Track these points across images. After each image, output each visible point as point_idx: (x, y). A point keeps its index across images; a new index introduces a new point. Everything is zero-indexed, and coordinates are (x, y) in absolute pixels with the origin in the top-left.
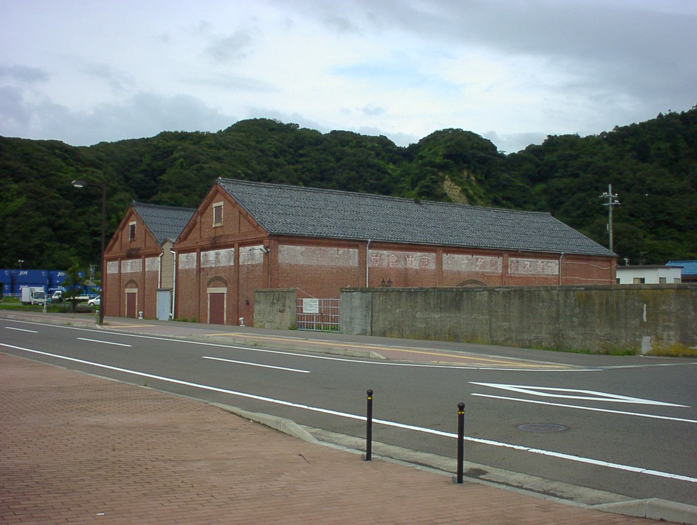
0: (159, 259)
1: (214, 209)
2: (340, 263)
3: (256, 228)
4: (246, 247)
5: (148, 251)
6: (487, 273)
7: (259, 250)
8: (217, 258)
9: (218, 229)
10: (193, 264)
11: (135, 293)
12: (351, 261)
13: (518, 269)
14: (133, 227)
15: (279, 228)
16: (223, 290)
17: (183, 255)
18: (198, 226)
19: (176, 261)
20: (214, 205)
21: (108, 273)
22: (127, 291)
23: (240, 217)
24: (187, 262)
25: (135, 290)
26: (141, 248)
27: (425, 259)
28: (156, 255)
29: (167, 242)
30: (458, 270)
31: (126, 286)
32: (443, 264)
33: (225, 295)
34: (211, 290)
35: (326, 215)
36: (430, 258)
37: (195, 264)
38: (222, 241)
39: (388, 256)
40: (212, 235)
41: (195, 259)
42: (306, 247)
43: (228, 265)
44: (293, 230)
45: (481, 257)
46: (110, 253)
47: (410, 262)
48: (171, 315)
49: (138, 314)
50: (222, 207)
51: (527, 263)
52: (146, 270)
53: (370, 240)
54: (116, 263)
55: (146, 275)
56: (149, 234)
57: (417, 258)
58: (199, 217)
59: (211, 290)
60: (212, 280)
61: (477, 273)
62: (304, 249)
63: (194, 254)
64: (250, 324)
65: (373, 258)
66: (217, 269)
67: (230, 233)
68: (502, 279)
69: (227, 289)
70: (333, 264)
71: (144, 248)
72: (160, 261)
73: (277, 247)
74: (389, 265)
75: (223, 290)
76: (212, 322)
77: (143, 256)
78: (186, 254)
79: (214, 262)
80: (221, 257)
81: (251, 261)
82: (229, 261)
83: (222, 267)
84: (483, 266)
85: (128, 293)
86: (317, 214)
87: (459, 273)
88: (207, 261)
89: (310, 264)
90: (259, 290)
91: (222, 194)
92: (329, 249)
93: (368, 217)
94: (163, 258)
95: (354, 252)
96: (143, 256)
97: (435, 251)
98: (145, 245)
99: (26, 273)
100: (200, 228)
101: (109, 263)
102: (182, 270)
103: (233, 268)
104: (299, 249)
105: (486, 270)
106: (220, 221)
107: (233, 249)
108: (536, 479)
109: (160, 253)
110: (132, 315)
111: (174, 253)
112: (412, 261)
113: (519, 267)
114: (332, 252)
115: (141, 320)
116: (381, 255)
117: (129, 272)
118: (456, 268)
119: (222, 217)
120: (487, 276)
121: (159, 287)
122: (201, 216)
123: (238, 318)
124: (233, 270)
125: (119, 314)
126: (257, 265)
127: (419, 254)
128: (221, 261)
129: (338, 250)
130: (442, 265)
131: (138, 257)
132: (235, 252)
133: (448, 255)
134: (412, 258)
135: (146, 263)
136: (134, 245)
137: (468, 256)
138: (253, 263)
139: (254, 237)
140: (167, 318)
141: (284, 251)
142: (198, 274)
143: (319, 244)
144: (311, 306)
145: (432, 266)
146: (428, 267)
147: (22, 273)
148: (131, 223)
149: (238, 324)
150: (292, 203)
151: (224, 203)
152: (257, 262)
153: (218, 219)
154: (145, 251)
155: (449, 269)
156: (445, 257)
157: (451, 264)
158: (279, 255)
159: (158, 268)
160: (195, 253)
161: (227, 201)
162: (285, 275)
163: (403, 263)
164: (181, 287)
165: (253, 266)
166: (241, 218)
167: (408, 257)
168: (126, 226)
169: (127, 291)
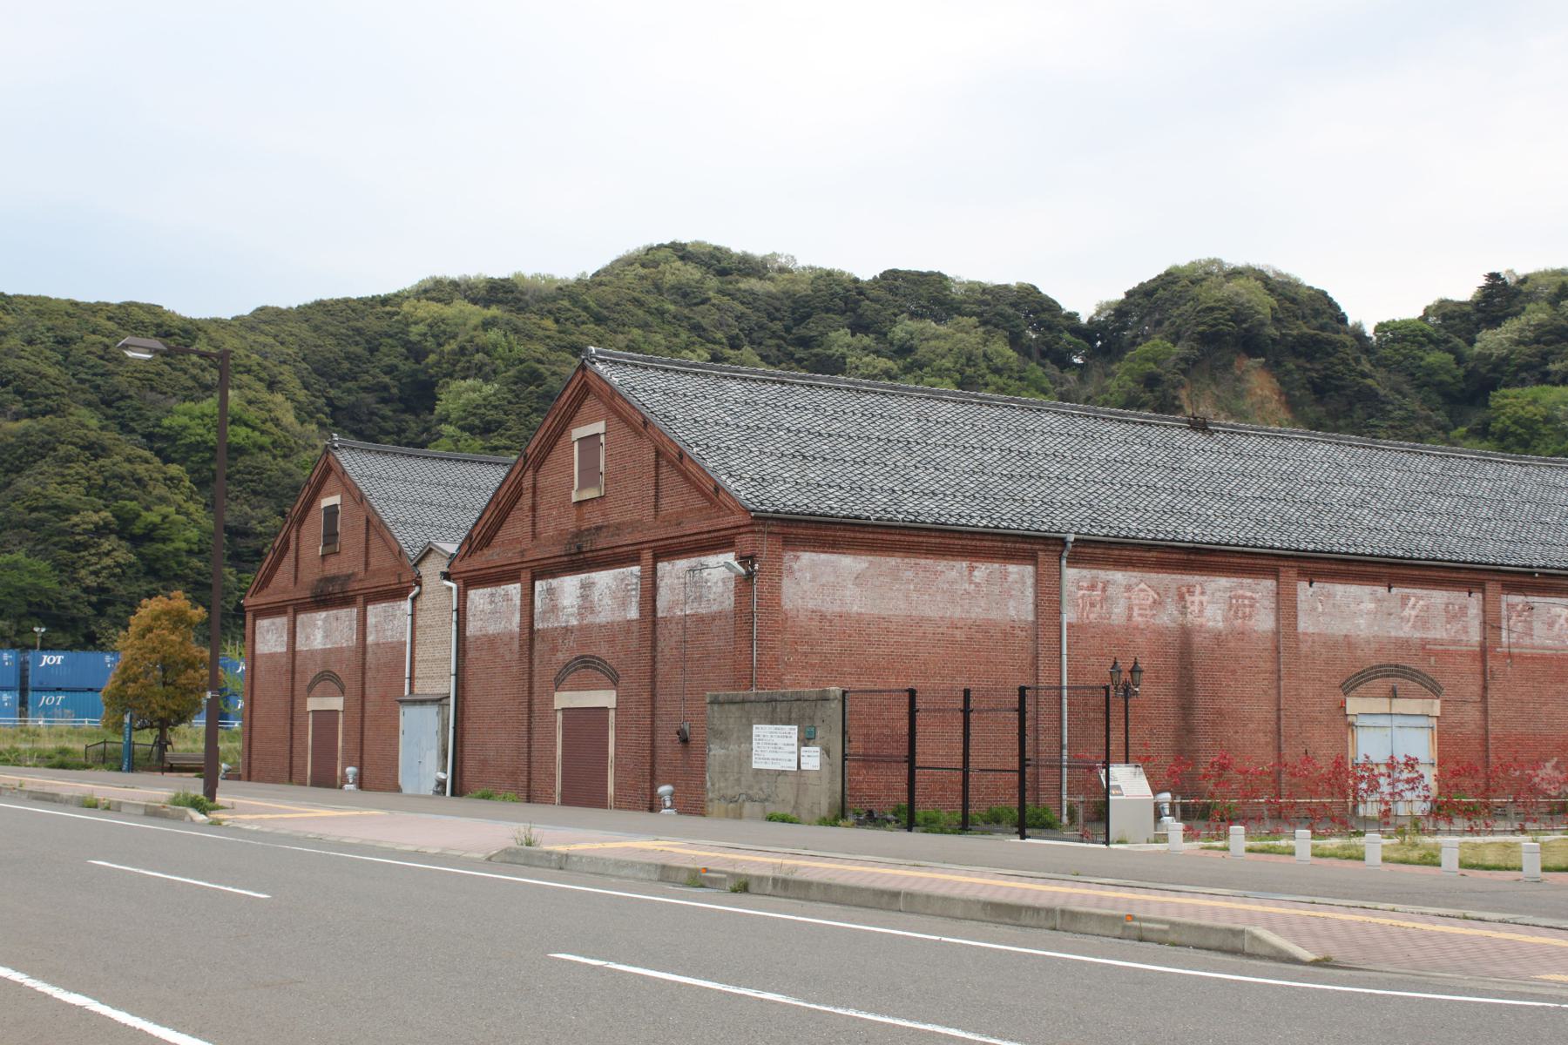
0: (406, 605)
1: (576, 445)
2: (978, 611)
3: (710, 500)
4: (677, 562)
5: (374, 582)
6: (1435, 641)
7: (720, 568)
8: (584, 597)
9: (586, 509)
10: (509, 621)
11: (336, 711)
12: (1012, 603)
13: (1531, 629)
14: (331, 512)
15: (785, 496)
16: (605, 698)
17: (481, 591)
18: (526, 500)
19: (457, 610)
20: (578, 433)
21: (257, 652)
22: (313, 704)
23: (657, 466)
24: (493, 612)
25: (336, 703)
26: (353, 574)
27: (1244, 597)
28: (397, 594)
29: (432, 555)
30: (1344, 632)
31: (310, 691)
32: (1300, 614)
33: (612, 714)
34: (565, 699)
35: (925, 463)
36: (1256, 596)
37: (517, 618)
38: (602, 542)
39: (1129, 588)
40: (570, 524)
41: (518, 602)
42: (870, 558)
43: (620, 619)
44: (833, 504)
45: (1418, 592)
46: (265, 592)
47: (1196, 608)
48: (443, 776)
49: (344, 775)
50: (602, 439)
51: (1558, 610)
52: (371, 639)
53: (1071, 538)
54: (282, 622)
55: (369, 656)
56: (378, 533)
57: (1218, 594)
58: (530, 473)
59: (565, 699)
60: (568, 668)
61: (1403, 644)
62: (867, 565)
63: (514, 589)
64: (692, 805)
65: (1081, 592)
66: (584, 630)
67: (627, 518)
68: (1484, 661)
69: (617, 696)
70: (957, 613)
71: (362, 575)
72: (409, 612)
73: (780, 558)
74: (1130, 618)
75: (605, 698)
76: (569, 799)
77: (360, 600)
78: (489, 590)
79: (575, 610)
80: (597, 594)
81: (695, 604)
82: (624, 605)
83: (600, 626)
84: (1423, 621)
85: (313, 711)
86: (898, 456)
87: (1349, 644)
88: (554, 609)
89: (885, 613)
90: (723, 694)
91: (600, 398)
92: (942, 565)
93: (1055, 469)
94: (418, 605)
95: (1020, 575)
96: (360, 600)
97: (1274, 573)
98: (367, 564)
99: (58, 659)
100: (534, 508)
101: (263, 624)
102: (478, 638)
103: (635, 628)
104: (850, 563)
105: (1430, 635)
106: (595, 484)
107: (636, 569)
108: (44, 566)
109: (412, 588)
110: (326, 779)
111: (453, 585)
112: (1201, 603)
113: (1534, 624)
114: (954, 574)
115: (350, 791)
116: (1106, 584)
117: (320, 647)
118: (1338, 628)
119: (602, 469)
120: (1436, 654)
121: (407, 693)
122: (536, 471)
123: (653, 788)
124: (636, 635)
125: (289, 775)
126: (714, 617)
127: (1223, 582)
128: (598, 609)
129: (972, 569)
130: (1296, 617)
131: (345, 601)
132: (641, 578)
133: (1314, 584)
134: (1203, 593)
135: (371, 620)
136: (334, 567)
137: (1375, 588)
138: (703, 611)
139: (705, 526)
140: (429, 787)
141: (799, 570)
142: (526, 648)
143: (910, 549)
144: (776, 748)
145: (1264, 621)
146: (1252, 622)
147: (47, 659)
148: (326, 502)
149: (653, 806)
150: (820, 424)
151: (607, 425)
152: (715, 608)
153: (589, 474)
154: (367, 584)
155: (1316, 631)
156: (1304, 590)
157: (1323, 613)
158: (786, 583)
159: (403, 634)
160: (518, 585)
161: (615, 419)
162: (806, 648)
163: (1172, 608)
164: (474, 688)
165: (700, 619)
166: (664, 470)
167: (1188, 592)
168: (312, 512)
169: (313, 704)
